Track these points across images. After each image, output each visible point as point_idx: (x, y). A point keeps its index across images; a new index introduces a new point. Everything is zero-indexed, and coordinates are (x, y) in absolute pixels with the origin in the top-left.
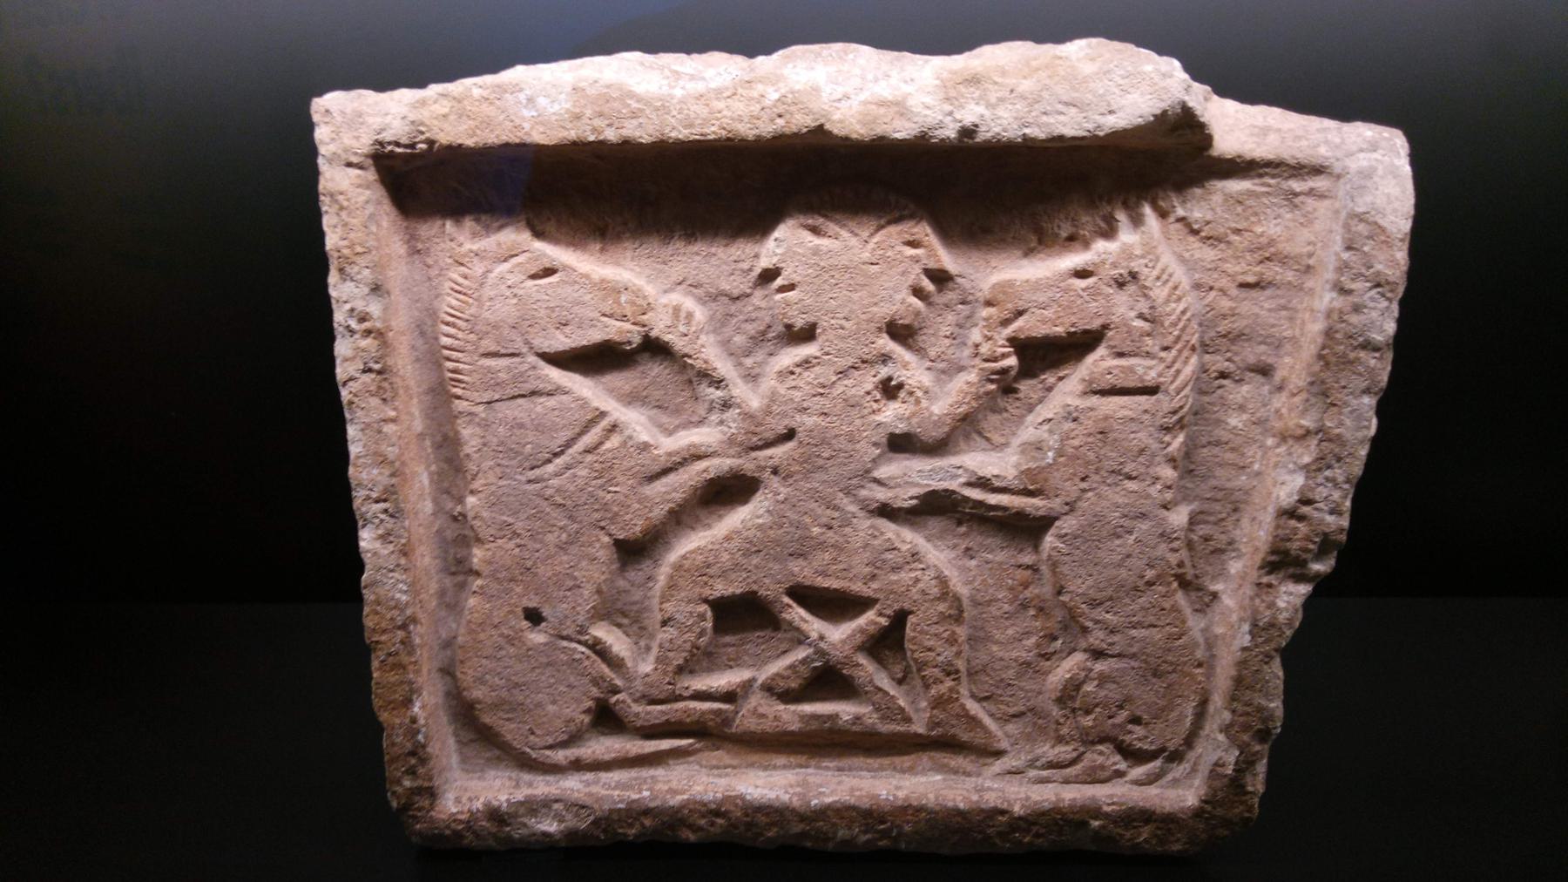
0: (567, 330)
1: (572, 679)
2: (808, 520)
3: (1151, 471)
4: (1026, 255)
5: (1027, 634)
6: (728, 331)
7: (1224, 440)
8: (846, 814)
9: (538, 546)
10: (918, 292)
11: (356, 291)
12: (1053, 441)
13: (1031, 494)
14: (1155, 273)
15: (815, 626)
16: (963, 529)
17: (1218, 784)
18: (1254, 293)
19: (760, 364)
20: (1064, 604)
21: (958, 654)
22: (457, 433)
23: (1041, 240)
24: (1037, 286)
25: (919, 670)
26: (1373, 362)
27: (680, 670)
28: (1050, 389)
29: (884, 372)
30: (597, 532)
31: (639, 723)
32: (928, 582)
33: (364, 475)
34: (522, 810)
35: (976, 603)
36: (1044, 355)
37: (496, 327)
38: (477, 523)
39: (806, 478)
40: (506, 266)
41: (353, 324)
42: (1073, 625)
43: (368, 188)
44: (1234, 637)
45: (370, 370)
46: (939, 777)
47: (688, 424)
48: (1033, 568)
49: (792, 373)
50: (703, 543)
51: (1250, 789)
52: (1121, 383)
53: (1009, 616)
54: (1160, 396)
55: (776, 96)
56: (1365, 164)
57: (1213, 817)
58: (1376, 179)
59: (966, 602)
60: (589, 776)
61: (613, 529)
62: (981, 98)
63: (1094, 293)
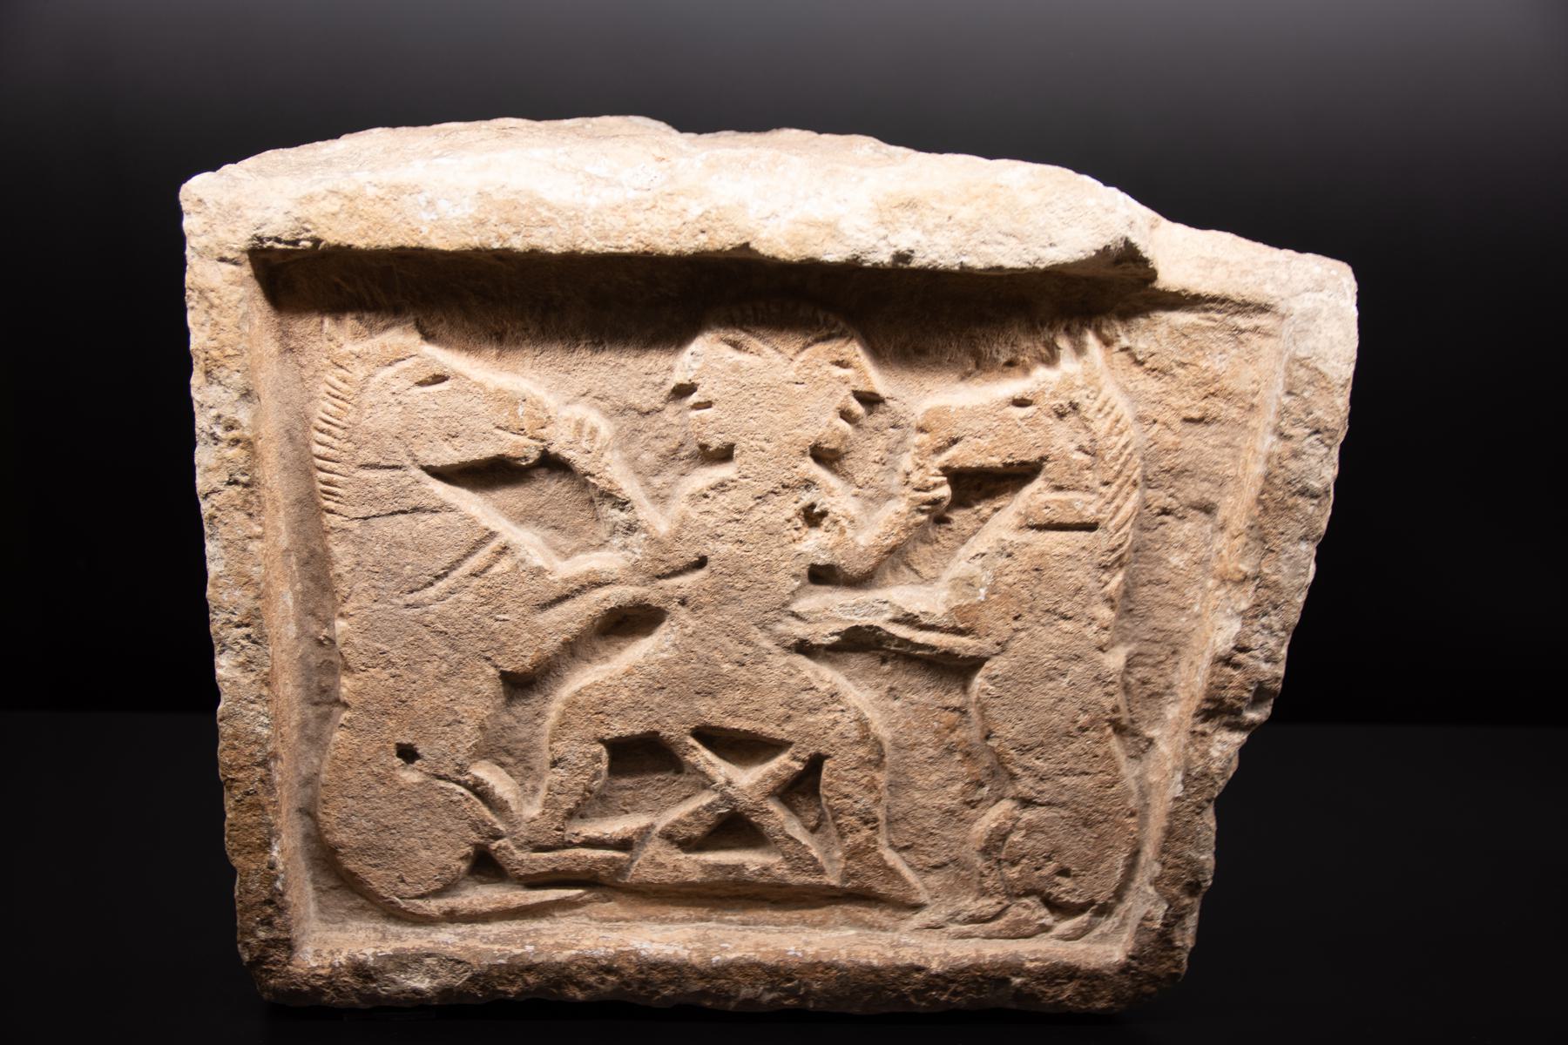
0: (456, 442)
1: (449, 822)
2: (717, 655)
3: (1088, 611)
4: (962, 379)
5: (953, 780)
6: (635, 448)
7: (1165, 578)
8: (749, 972)
9: (415, 677)
10: (846, 415)
11: (224, 396)
12: (986, 578)
13: (961, 632)
14: (1097, 405)
15: (720, 769)
16: (887, 668)
17: (1145, 939)
18: (1198, 428)
19: (670, 485)
20: (992, 749)
21: (878, 800)
22: (327, 550)
23: (980, 364)
24: (973, 414)
25: (834, 818)
26: (1310, 509)
27: (570, 815)
28: (984, 521)
29: (807, 498)
30: (483, 663)
31: (523, 872)
32: (847, 725)
33: (224, 594)
34: (390, 966)
35: (898, 747)
36: (978, 485)
37: (376, 436)
38: (347, 650)
39: (717, 610)
40: (391, 371)
41: (219, 431)
42: (1001, 772)
43: (242, 285)
44: (1167, 786)
45: (236, 482)
46: (852, 932)
47: (587, 548)
48: (961, 710)
49: (706, 496)
50: (600, 678)
51: (1179, 944)
52: (1057, 518)
53: (933, 761)
54: (1098, 533)
55: (699, 211)
56: (1309, 305)
57: (1140, 973)
58: (1319, 321)
59: (887, 746)
60: (465, 929)
61: (499, 660)
62: (917, 223)
63: (1033, 423)
